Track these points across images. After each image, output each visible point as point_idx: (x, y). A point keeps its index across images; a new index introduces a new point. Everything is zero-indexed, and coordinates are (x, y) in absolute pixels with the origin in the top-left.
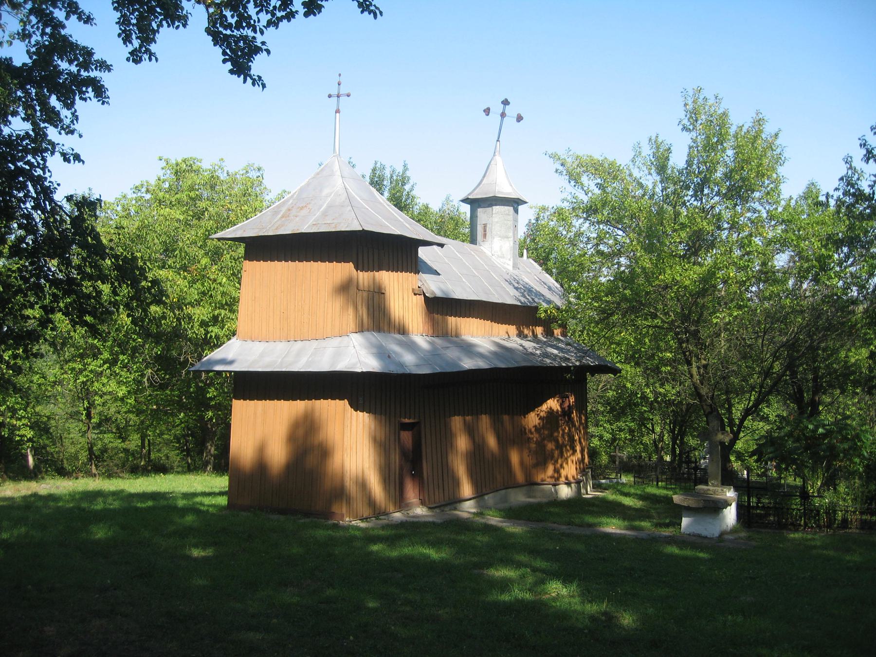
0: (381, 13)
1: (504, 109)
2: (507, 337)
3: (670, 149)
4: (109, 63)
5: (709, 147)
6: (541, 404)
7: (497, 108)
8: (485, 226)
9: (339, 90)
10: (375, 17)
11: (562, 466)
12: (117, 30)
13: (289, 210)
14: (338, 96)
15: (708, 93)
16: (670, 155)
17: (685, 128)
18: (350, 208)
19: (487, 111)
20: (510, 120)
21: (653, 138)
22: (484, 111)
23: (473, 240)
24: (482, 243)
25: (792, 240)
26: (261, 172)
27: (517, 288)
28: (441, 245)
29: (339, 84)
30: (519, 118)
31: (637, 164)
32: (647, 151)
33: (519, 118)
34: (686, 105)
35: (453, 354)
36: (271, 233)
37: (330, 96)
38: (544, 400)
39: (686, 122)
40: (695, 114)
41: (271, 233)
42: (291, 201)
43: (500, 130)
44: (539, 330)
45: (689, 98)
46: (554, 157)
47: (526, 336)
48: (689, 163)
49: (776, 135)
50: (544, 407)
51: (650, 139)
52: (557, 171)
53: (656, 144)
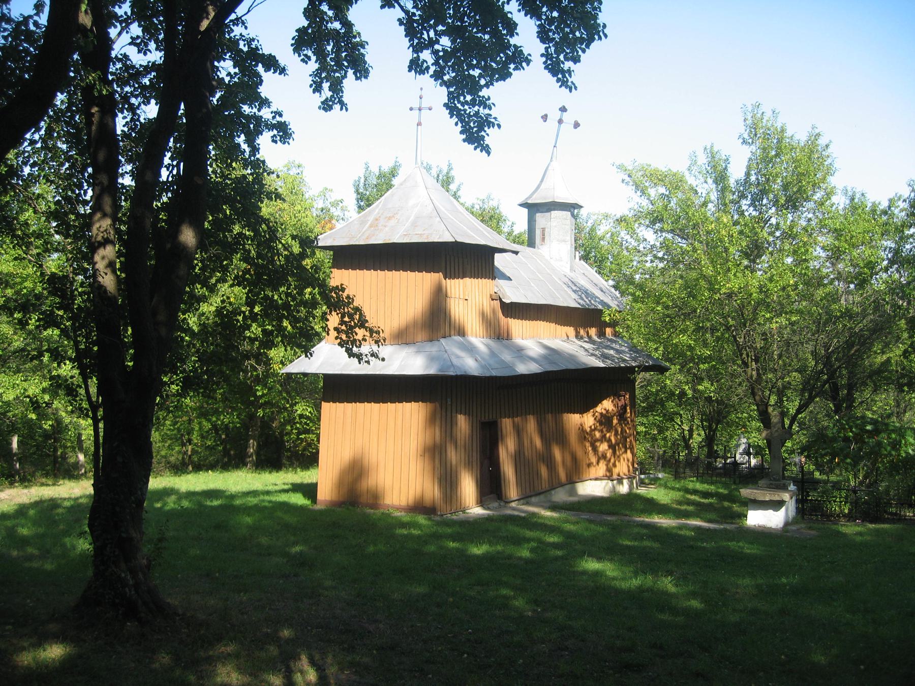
0: (576, 88)
1: (562, 116)
2: (566, 338)
3: (728, 160)
4: (270, 100)
5: (766, 160)
6: (596, 406)
7: (555, 115)
8: (543, 230)
9: (421, 103)
10: (571, 91)
11: (615, 465)
12: (309, 80)
13: (377, 220)
14: (420, 109)
15: (766, 109)
16: (728, 165)
17: (744, 142)
18: (438, 219)
19: (545, 118)
20: (567, 127)
21: (708, 147)
22: (542, 117)
23: (531, 243)
24: (540, 247)
25: (845, 249)
26: (301, 169)
27: (574, 291)
28: (516, 253)
29: (421, 98)
30: (577, 125)
31: (693, 172)
32: (703, 160)
33: (577, 125)
34: (745, 120)
35: (507, 357)
36: (362, 242)
37: (411, 109)
38: (600, 401)
39: (746, 136)
40: (755, 129)
41: (362, 243)
42: (377, 211)
43: (557, 136)
44: (593, 332)
45: (748, 114)
46: (621, 167)
47: (582, 338)
48: (748, 174)
49: (827, 146)
50: (599, 409)
51: (705, 148)
52: (623, 181)
53: (712, 156)
